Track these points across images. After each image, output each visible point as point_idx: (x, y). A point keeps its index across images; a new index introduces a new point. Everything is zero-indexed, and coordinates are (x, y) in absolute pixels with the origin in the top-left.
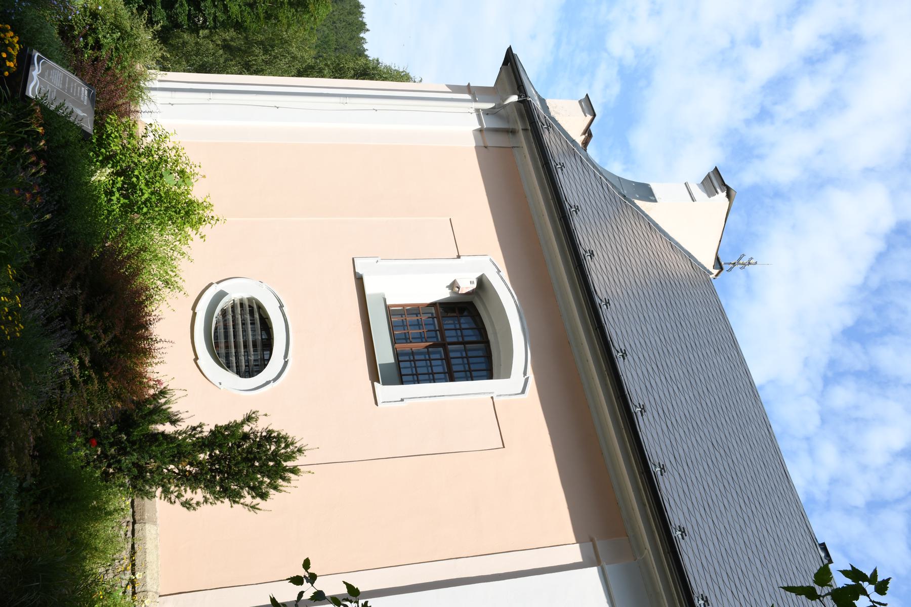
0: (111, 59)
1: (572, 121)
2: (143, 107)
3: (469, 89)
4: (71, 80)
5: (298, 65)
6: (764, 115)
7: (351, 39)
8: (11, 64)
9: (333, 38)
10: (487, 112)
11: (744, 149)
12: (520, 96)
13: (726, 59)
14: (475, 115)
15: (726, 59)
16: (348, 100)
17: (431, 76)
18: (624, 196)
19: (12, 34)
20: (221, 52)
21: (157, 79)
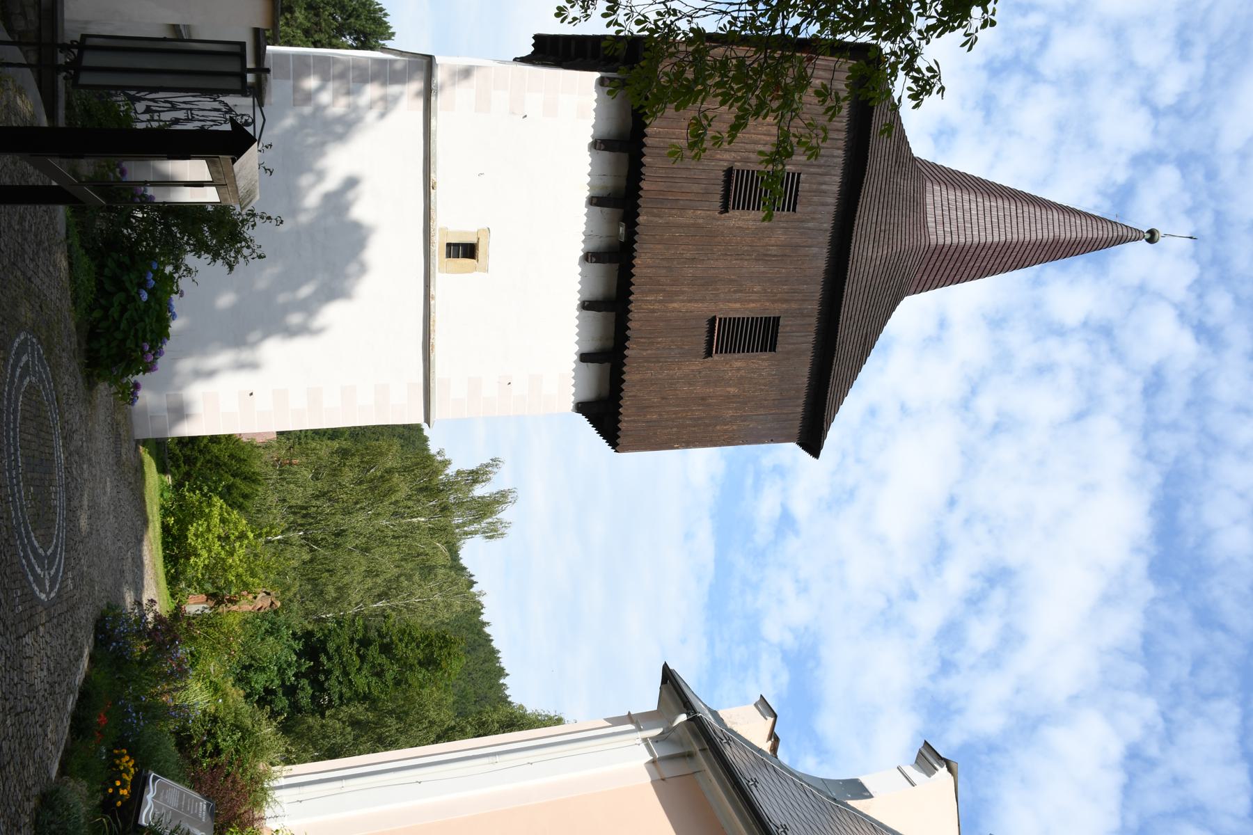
0: (231, 763)
1: (754, 730)
2: (268, 812)
3: (630, 718)
4: (188, 796)
5: (437, 729)
6: (946, 667)
7: (491, 688)
8: (124, 792)
9: (471, 690)
10: (656, 740)
11: (938, 709)
12: (688, 714)
13: (888, 619)
14: (643, 746)
15: (888, 619)
16: (498, 758)
17: (581, 713)
18: (835, 800)
19: (127, 758)
20: (349, 729)
21: (284, 774)
